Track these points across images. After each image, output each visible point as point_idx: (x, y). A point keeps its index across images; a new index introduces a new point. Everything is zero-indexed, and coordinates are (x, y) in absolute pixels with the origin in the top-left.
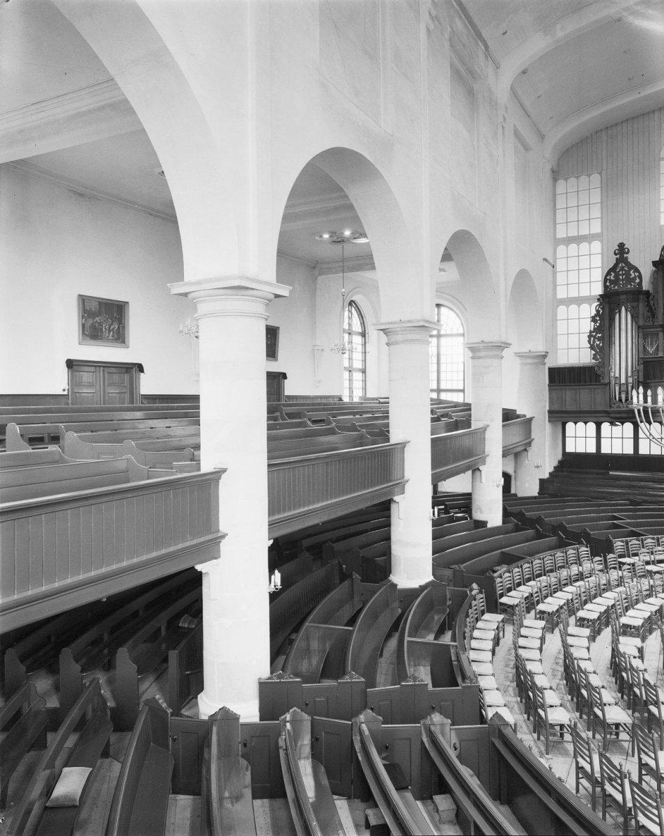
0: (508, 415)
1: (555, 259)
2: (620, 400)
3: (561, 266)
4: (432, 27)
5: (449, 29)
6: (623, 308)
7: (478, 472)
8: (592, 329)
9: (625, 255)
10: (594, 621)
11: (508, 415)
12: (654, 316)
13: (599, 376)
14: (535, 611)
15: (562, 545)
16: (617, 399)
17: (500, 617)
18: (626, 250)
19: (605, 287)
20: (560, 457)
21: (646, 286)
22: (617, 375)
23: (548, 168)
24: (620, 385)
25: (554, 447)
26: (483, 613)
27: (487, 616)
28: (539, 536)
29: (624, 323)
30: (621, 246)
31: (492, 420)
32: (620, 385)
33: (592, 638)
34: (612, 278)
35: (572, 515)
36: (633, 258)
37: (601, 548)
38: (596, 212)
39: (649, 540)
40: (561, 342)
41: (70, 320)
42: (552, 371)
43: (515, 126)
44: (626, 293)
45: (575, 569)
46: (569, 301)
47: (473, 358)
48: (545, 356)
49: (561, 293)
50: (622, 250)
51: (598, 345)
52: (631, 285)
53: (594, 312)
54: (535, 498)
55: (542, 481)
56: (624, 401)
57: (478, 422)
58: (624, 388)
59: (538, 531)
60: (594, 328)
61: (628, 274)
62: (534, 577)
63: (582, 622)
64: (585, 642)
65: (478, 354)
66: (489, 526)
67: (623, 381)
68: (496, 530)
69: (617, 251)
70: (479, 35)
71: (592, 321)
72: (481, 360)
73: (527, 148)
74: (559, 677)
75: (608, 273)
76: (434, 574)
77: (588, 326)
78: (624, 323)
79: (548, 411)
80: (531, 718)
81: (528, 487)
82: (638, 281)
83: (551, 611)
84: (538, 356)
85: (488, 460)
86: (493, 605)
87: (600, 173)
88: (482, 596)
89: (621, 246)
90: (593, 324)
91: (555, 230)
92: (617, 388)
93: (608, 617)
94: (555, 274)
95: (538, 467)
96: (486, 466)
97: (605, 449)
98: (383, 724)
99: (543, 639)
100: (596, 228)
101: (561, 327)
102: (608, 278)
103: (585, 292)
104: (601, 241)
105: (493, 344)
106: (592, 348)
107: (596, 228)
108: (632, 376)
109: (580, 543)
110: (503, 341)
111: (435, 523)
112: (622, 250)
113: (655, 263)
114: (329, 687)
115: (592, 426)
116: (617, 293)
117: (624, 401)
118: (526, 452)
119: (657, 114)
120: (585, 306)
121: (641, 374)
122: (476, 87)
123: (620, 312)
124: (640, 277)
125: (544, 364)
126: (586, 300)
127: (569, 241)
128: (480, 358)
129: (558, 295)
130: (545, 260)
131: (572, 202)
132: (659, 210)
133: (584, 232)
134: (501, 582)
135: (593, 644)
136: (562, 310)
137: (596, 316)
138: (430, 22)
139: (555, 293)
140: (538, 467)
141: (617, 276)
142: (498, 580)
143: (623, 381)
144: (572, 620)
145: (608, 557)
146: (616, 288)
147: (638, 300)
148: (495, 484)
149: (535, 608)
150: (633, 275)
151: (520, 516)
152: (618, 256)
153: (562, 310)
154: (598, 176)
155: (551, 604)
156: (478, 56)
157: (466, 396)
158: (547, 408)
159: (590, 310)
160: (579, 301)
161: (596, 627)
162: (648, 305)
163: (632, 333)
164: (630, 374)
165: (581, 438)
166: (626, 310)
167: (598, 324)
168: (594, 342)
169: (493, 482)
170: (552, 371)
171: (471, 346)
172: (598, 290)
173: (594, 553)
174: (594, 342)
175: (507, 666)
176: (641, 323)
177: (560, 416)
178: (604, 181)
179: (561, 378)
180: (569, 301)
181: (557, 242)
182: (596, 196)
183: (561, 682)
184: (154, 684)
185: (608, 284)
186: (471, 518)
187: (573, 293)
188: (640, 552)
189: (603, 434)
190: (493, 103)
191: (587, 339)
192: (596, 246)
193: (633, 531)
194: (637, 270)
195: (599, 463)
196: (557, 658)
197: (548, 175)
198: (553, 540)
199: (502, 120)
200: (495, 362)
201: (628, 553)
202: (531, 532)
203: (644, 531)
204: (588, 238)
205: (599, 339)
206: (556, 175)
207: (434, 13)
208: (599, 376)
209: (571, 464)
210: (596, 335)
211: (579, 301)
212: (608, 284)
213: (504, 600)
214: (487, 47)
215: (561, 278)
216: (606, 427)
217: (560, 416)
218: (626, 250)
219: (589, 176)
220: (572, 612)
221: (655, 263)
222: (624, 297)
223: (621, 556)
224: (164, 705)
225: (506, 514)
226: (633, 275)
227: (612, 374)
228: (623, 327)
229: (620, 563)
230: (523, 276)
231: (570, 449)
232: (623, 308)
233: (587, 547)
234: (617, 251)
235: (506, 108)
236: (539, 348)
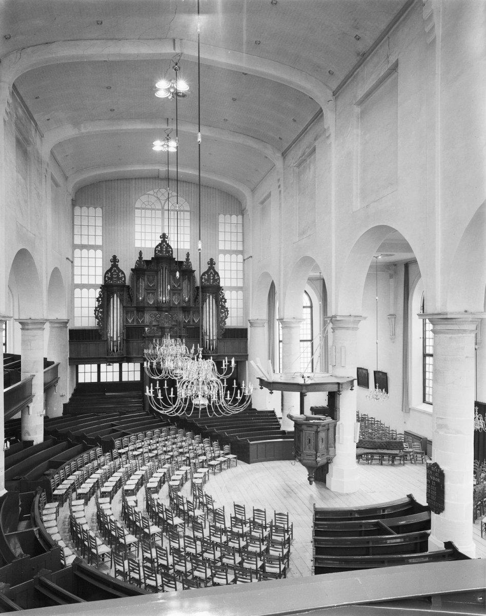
0: (47, 363)
1: (73, 257)
2: (113, 351)
3: (77, 262)
4: (7, 119)
5: (15, 116)
6: (115, 295)
7: (27, 408)
8: (97, 306)
9: (117, 263)
10: (86, 494)
11: (47, 363)
12: (131, 300)
13: (101, 335)
14: (77, 493)
15: (85, 449)
17: (57, 503)
19: (105, 281)
20: (75, 386)
21: (128, 282)
22: (112, 336)
23: (70, 198)
24: (113, 341)
25: (71, 380)
26: (45, 504)
27: (47, 506)
28: (70, 445)
29: (116, 304)
30: (115, 257)
31: (37, 372)
32: (113, 341)
33: (86, 504)
35: (87, 426)
36: (121, 265)
37: (108, 447)
38: (99, 231)
39: (133, 437)
40: (77, 312)
42: (71, 331)
43: (52, 174)
44: (117, 286)
45: (95, 463)
46: (82, 286)
47: (22, 329)
48: (67, 323)
49: (77, 280)
50: (115, 260)
51: (100, 316)
52: (120, 282)
53: (98, 296)
54: (61, 417)
55: (64, 405)
56: (115, 351)
57: (27, 374)
58: (115, 344)
59: (69, 441)
61: (118, 275)
62: (71, 473)
63: (79, 497)
64: (82, 507)
65: (27, 327)
66: (35, 443)
67: (115, 339)
68: (40, 447)
70: (32, 118)
71: (97, 301)
72: (29, 331)
73: (57, 185)
74: (96, 529)
75: (107, 273)
76: (6, 488)
77: (94, 304)
78: (116, 304)
79: (69, 358)
80: (131, 529)
81: (58, 411)
82: (123, 279)
83: (86, 492)
84: (63, 322)
85: (34, 399)
86: (51, 498)
87: (102, 208)
88: (44, 493)
89: (115, 257)
90: (97, 303)
91: (73, 238)
92: (112, 343)
93: (98, 484)
94: (73, 267)
95: (62, 396)
96: (33, 403)
97: (103, 380)
98: (11, 587)
99: (57, 513)
100: (99, 242)
101: (77, 302)
102: (107, 275)
103: (92, 282)
104: (102, 251)
105: (38, 321)
106: (97, 317)
107: (99, 242)
108: (120, 336)
109: (97, 446)
110: (45, 318)
111: (7, 453)
112: (115, 260)
113: (132, 270)
115: (95, 367)
116: (112, 286)
117: (115, 351)
118: (54, 387)
119: (133, 181)
120: (92, 290)
121: (125, 335)
122: (29, 149)
123: (113, 297)
124: (125, 277)
125: (67, 327)
126: (93, 286)
127: (82, 247)
128: (28, 329)
129: (75, 281)
130: (67, 258)
131: (85, 223)
132: (134, 230)
133: (92, 243)
134: (54, 481)
135: (86, 507)
136: (77, 291)
137: (99, 297)
138: (5, 115)
139: (73, 280)
140: (62, 396)
141: (112, 275)
142: (52, 480)
143: (115, 339)
144: (74, 495)
145: (113, 451)
147: (123, 291)
148: (39, 414)
149: (76, 491)
150: (121, 276)
151: (54, 433)
153: (77, 291)
154: (101, 209)
155: (85, 488)
156: (31, 131)
157: (7, 347)
158: (68, 356)
159: (96, 293)
160: (88, 286)
161: (86, 497)
162: (129, 294)
164: (119, 335)
165: (88, 373)
166: (117, 296)
168: (98, 314)
169: (38, 413)
170: (71, 331)
171: (20, 321)
172: (100, 281)
173: (104, 452)
174: (98, 314)
175: (64, 532)
176: (125, 305)
177: (75, 361)
178: (104, 213)
179: (78, 337)
180: (82, 286)
181: (75, 247)
182: (99, 222)
183: (97, 532)
185: (107, 279)
186: (20, 440)
187: (85, 282)
188: (129, 445)
189: (102, 370)
190: (40, 161)
191: (94, 312)
192: (99, 253)
193: (123, 432)
194: (123, 273)
195: (99, 387)
196: (92, 519)
197: (70, 203)
198: (79, 446)
199: (45, 172)
200: (39, 332)
201: (122, 446)
202: (64, 443)
203: (129, 431)
204: (95, 247)
205: (101, 312)
206: (74, 203)
207: (8, 110)
208: (101, 335)
209: (82, 390)
211: (88, 286)
213: (56, 492)
214: (36, 124)
215: (77, 271)
216: (103, 366)
217: (75, 361)
219: (95, 208)
220: (74, 490)
221: (132, 270)
222: (116, 288)
223: (119, 449)
225: (46, 433)
226: (121, 276)
227: (109, 335)
228: (115, 306)
229: (119, 453)
230: (56, 271)
231: (81, 380)
232: (115, 295)
233: (100, 447)
235: (48, 164)
236: (63, 316)
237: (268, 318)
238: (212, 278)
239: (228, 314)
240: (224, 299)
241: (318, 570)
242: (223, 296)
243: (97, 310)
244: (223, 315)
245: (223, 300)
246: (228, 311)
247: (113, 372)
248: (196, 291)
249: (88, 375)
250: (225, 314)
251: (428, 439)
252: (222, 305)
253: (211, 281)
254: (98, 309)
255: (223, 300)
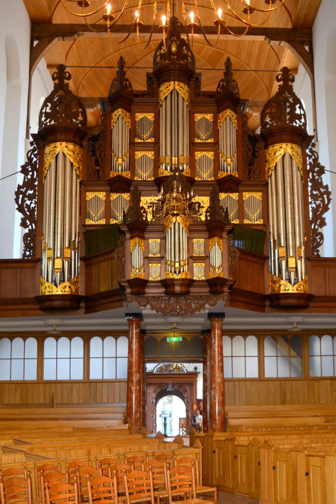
8: (21, 184)
16: (170, 271)
18: (67, 75)
34: (48, 110)
41: (188, 500)
60: (24, 182)
69: (55, 75)
82: (303, 120)
106: (21, 209)
114: (309, 215)
137: (27, 164)
146: (53, 122)
150: (74, 110)
152: (57, 81)
163: (302, 266)
167: (29, 177)
168: (23, 201)
174: (23, 201)
184: (278, 345)
205: (31, 197)
210: (26, 191)
212: (43, 119)
218: (67, 75)
224: (309, 191)
234: (55, 75)
237: (324, 377)
238: (288, 110)
239: (329, 200)
240: (318, 165)
241: (201, 74)
242: (316, 160)
243: (21, 193)
244: (318, 202)
245: (316, 169)
246: (329, 194)
247: (57, 358)
248: (251, 147)
249: (64, 364)
250: (323, 201)
251: (21, 222)
252: (315, 230)
253: (288, 117)
254: (23, 190)
255: (316, 169)
